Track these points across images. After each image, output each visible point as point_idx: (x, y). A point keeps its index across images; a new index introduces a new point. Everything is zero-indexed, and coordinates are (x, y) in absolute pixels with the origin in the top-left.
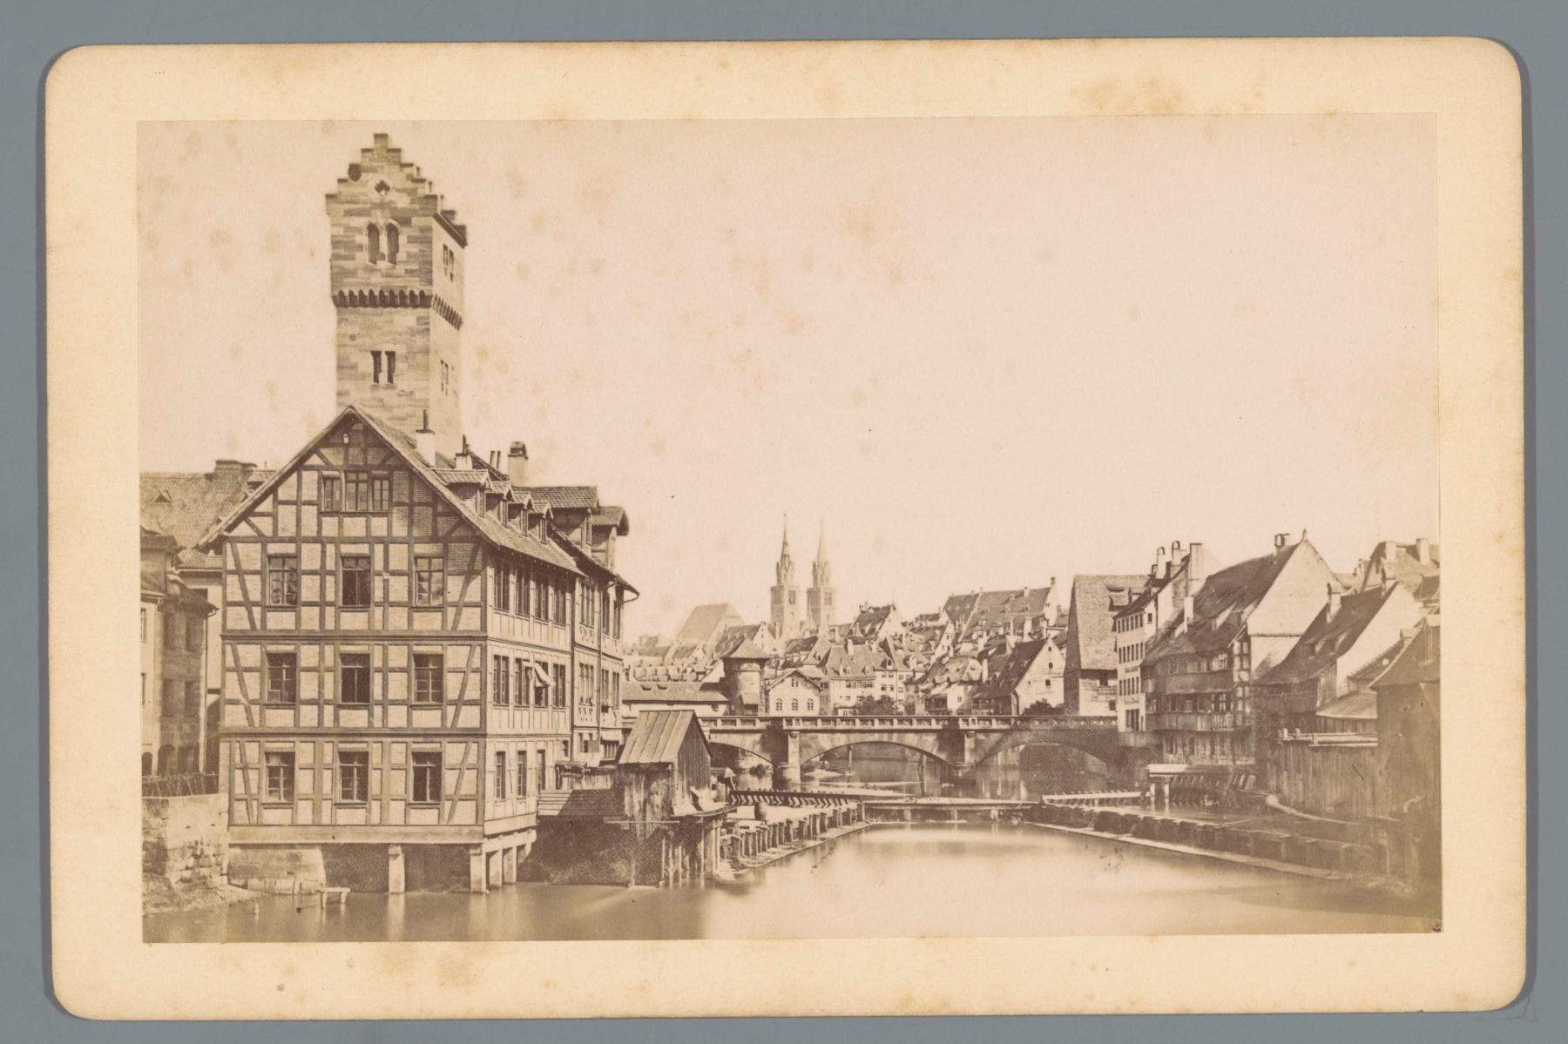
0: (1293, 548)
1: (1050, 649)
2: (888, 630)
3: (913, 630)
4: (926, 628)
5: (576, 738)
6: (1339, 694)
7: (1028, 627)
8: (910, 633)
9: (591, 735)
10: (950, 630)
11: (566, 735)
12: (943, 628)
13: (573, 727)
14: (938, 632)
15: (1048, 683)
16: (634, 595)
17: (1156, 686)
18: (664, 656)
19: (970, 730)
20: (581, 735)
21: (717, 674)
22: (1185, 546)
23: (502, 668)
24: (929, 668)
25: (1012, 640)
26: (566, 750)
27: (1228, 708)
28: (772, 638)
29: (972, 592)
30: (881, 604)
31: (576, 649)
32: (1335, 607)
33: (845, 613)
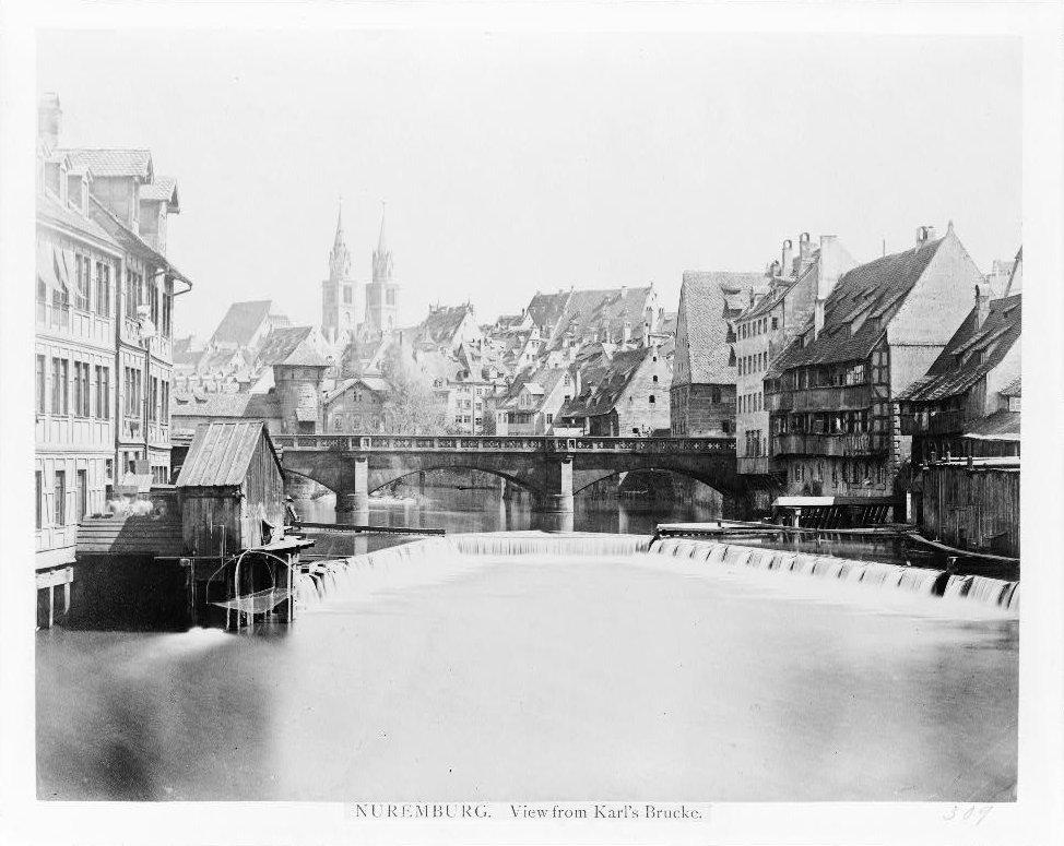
0: (938, 244)
1: (655, 359)
2: (468, 332)
3: (492, 336)
4: (507, 330)
5: (120, 455)
6: (987, 413)
7: (628, 335)
8: (489, 339)
9: (137, 454)
10: (536, 335)
11: (109, 453)
12: (527, 334)
13: (117, 444)
14: (522, 338)
15: (652, 399)
16: (186, 287)
17: (783, 402)
18: (196, 363)
19: (568, 453)
20: (126, 453)
21: (266, 383)
22: (814, 239)
23: (62, 373)
24: (512, 381)
25: (609, 348)
26: (109, 471)
27: (864, 427)
28: (325, 342)
29: (538, 293)
30: (455, 304)
31: (121, 348)
32: (983, 315)
33: (410, 313)
